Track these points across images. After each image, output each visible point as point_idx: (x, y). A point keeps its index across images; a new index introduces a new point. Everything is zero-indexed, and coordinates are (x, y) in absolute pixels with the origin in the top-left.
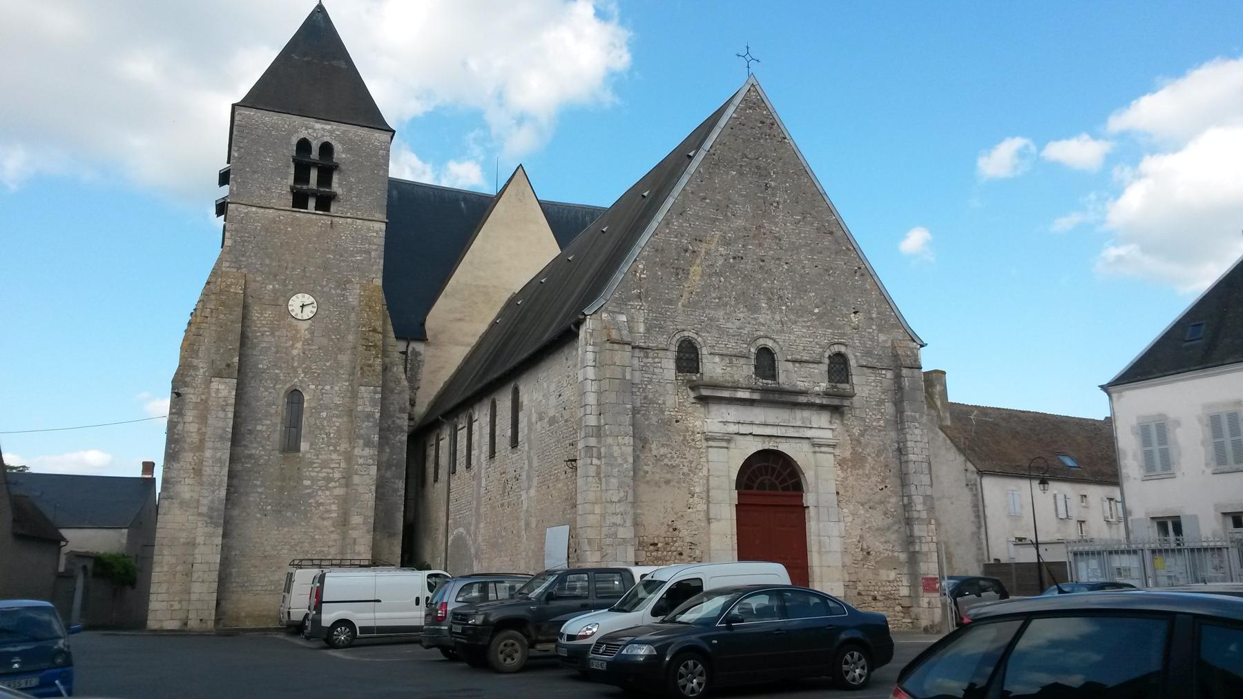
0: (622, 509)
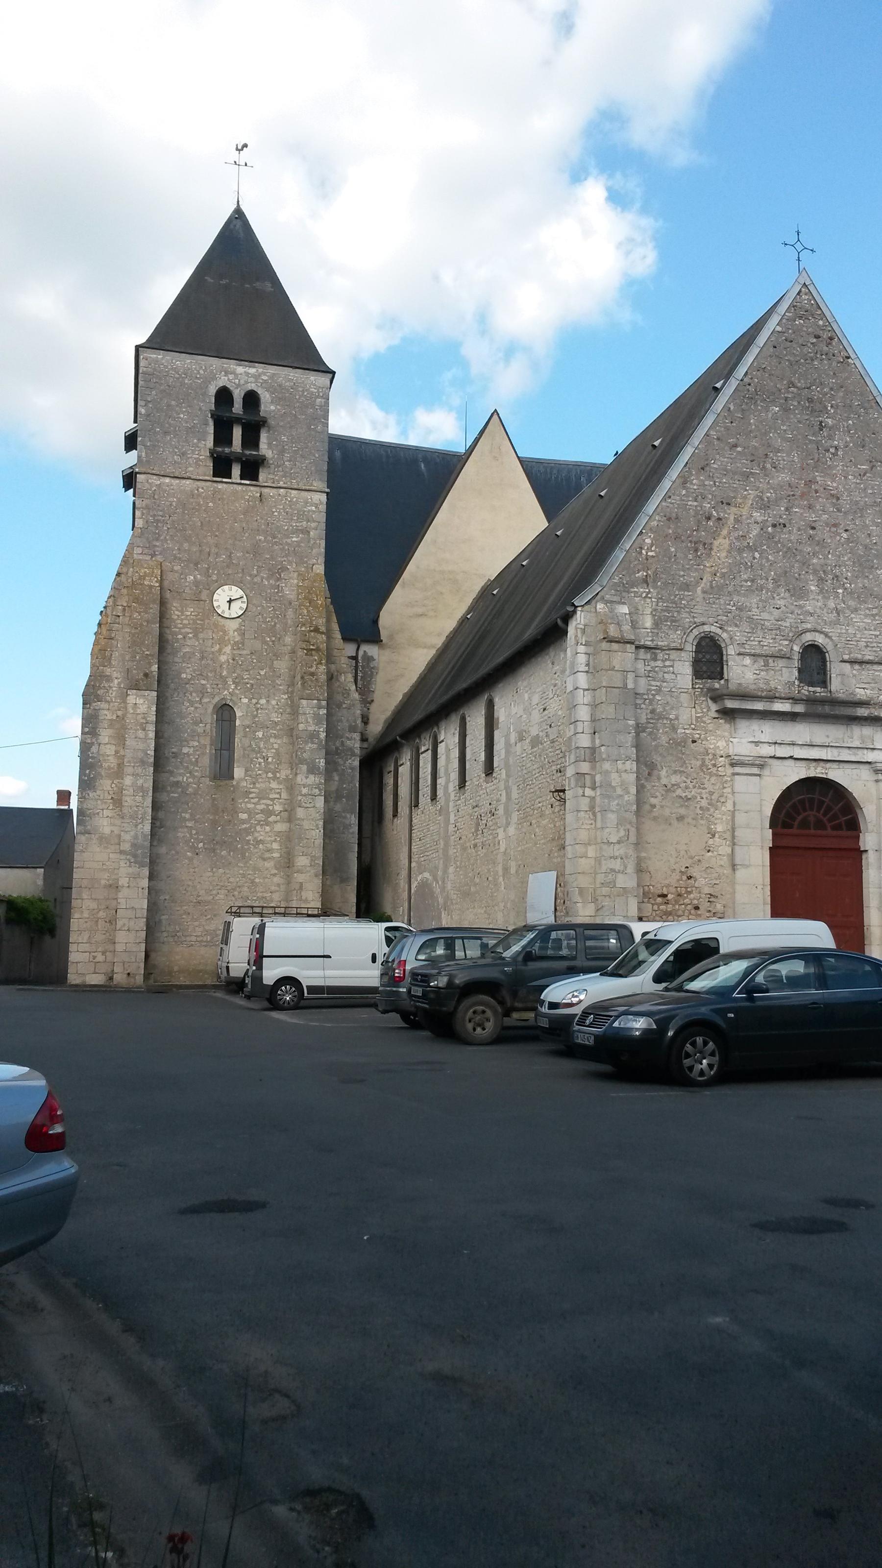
0: (622, 852)
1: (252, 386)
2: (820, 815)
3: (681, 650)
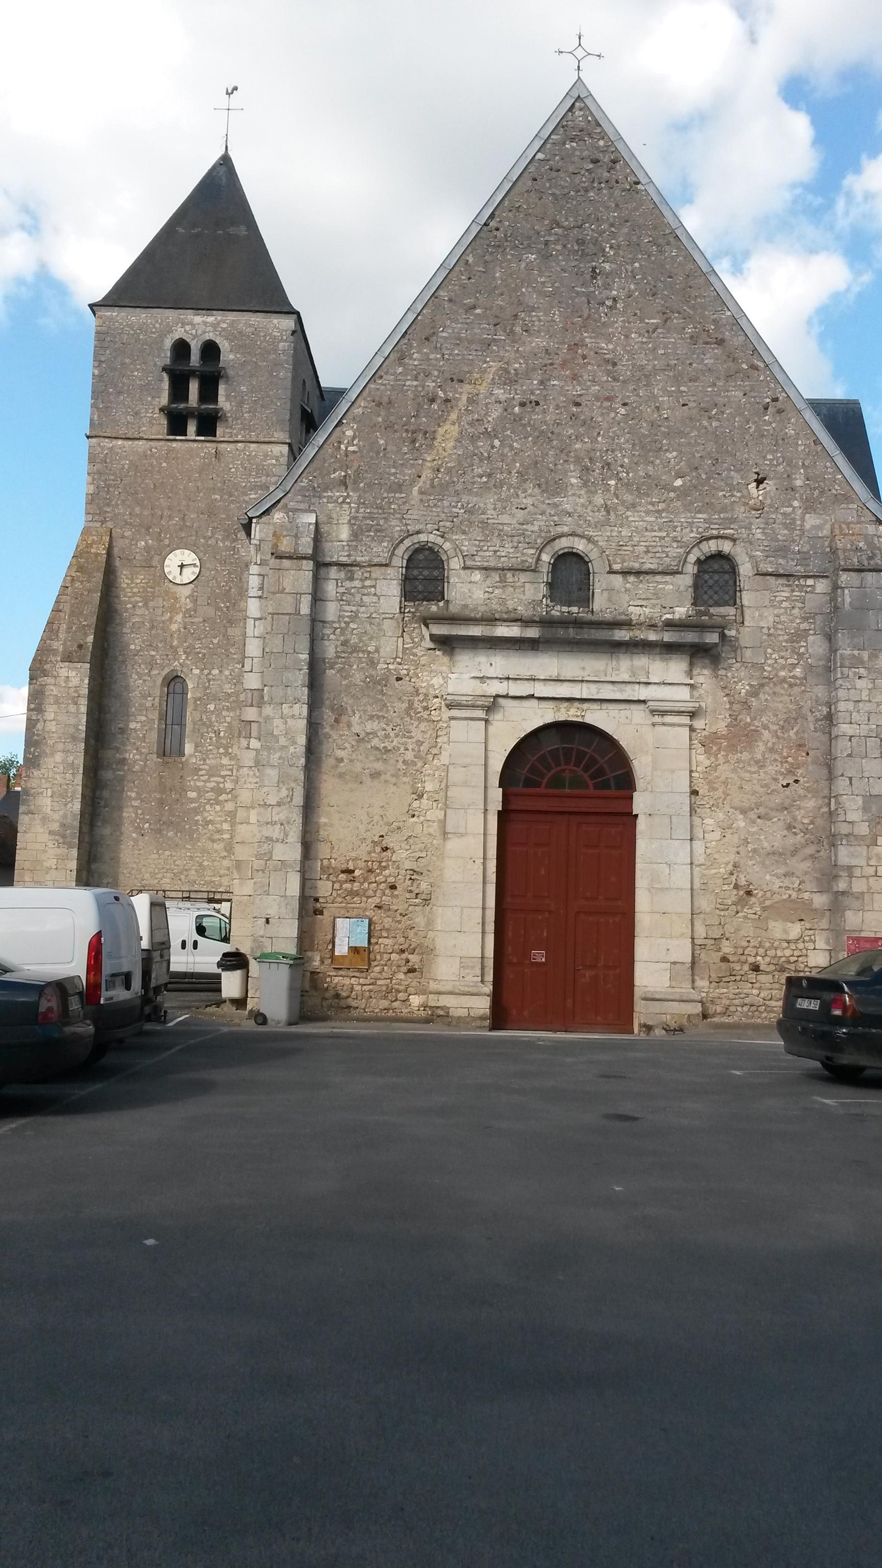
0: (282, 816)
3: (386, 565)
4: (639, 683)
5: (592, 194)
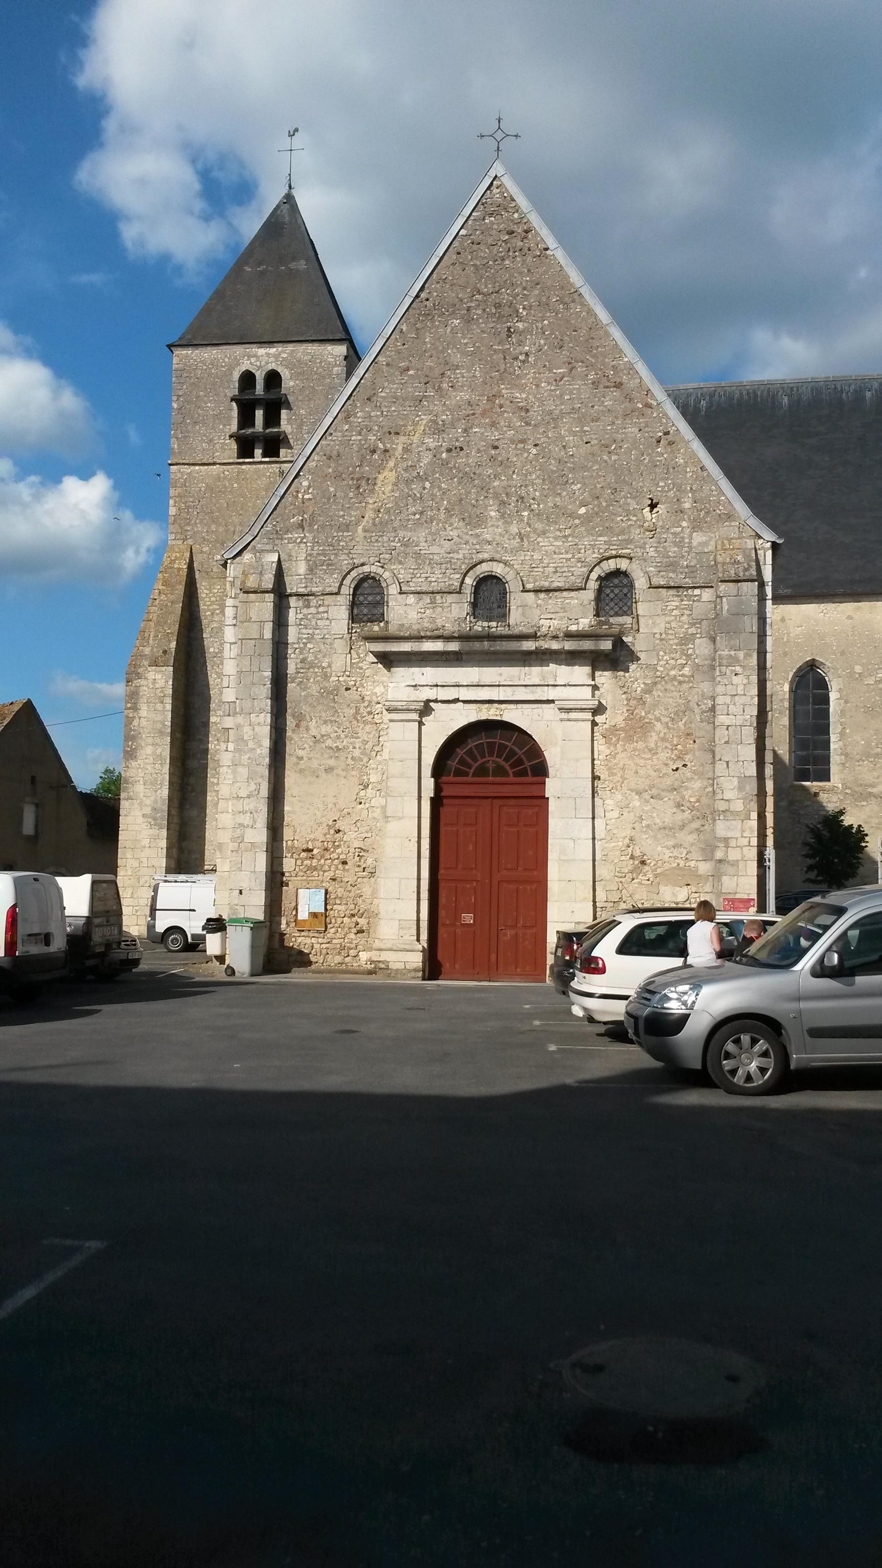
1: (272, 366)
2: (501, 761)
3: (336, 594)
4: (548, 685)
5: (507, 262)
